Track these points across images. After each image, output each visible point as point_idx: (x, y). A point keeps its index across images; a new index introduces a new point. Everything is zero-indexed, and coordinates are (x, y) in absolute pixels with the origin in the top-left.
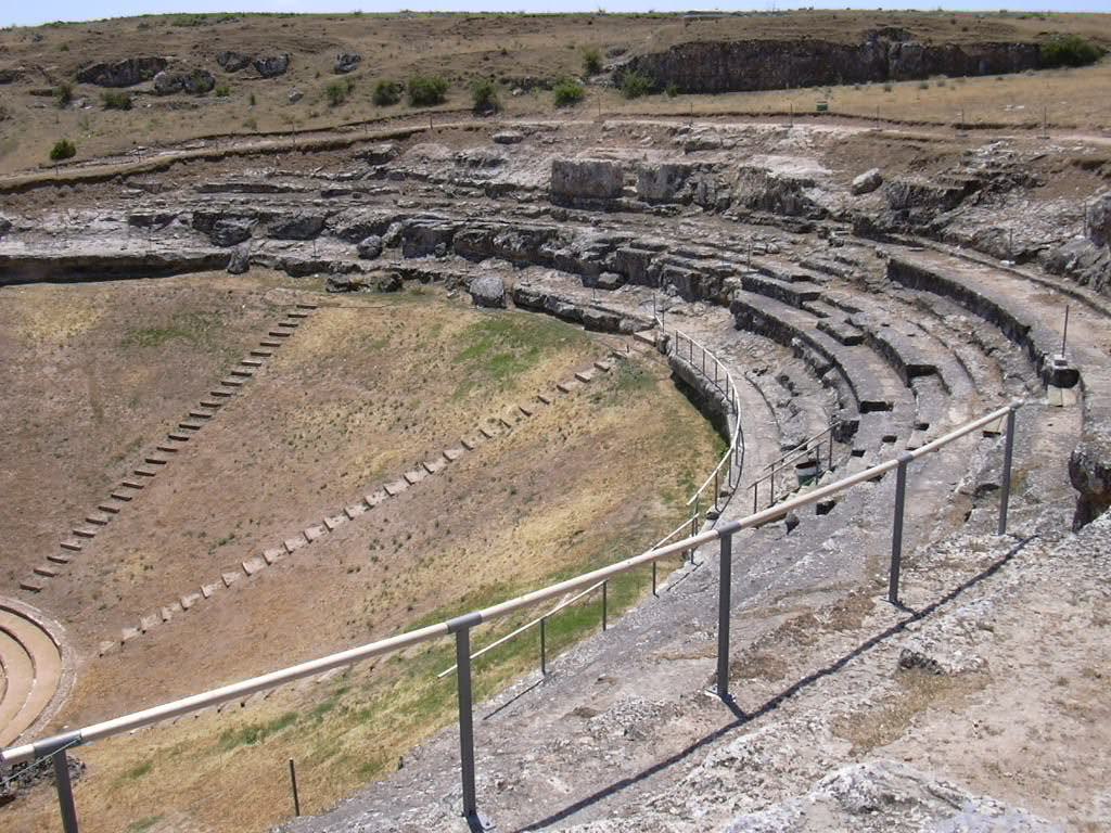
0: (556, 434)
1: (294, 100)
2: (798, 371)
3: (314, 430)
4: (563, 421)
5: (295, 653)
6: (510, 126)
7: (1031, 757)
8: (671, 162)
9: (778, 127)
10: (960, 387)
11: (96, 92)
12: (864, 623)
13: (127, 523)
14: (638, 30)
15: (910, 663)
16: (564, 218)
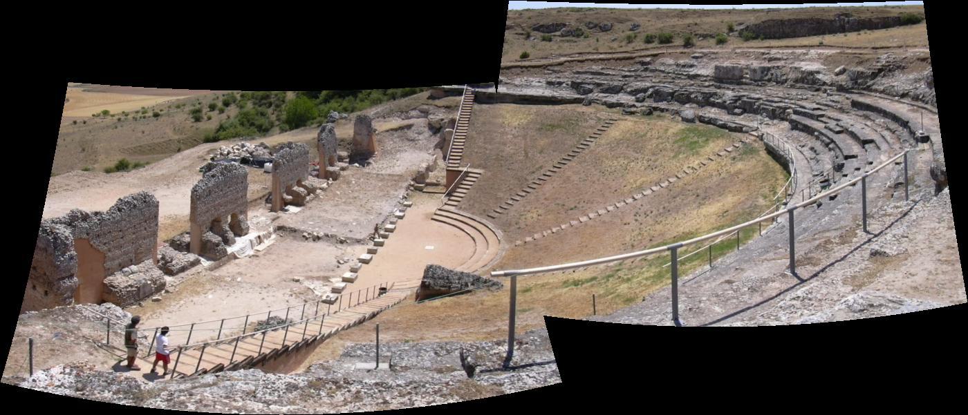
0: (716, 173)
1: (613, 40)
2: (818, 145)
3: (613, 168)
4: (720, 167)
5: (599, 254)
6: (698, 52)
7: (930, 282)
8: (762, 65)
9: (804, 51)
10: (884, 146)
11: (539, 35)
12: (853, 241)
13: (533, 197)
14: (749, 15)
15: (875, 254)
16: (719, 88)
